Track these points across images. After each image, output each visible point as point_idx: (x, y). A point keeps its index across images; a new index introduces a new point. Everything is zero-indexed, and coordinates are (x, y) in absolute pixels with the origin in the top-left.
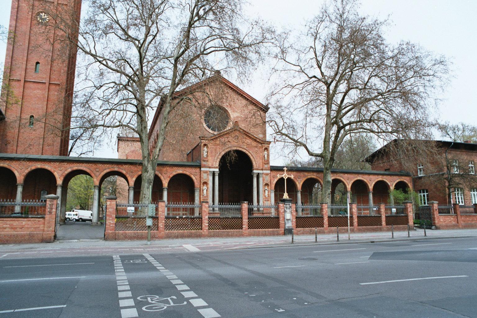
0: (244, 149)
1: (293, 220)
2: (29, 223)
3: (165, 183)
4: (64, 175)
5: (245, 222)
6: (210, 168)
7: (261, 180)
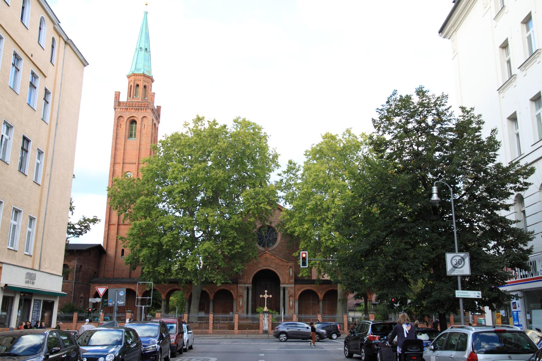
0: (272, 267)
3: (211, 297)
4: (143, 292)
6: (245, 284)
7: (286, 292)
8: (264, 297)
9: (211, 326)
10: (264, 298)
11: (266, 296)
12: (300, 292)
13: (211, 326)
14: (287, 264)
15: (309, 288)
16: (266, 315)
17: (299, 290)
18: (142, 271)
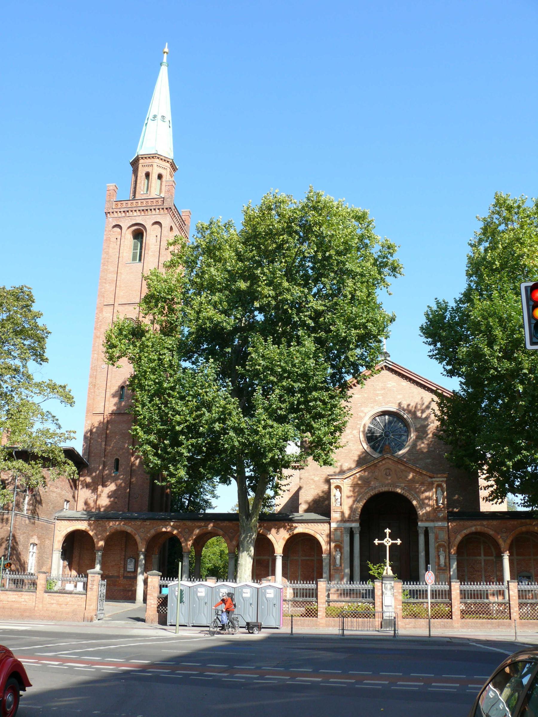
1: (398, 607)
2: (73, 599)
5: (321, 607)
7: (431, 536)
8: (383, 544)
9: (304, 558)
10: (382, 546)
11: (388, 542)
12: (459, 538)
13: (304, 558)
14: (430, 480)
15: (479, 528)
16: (388, 584)
17: (457, 531)
18: (130, 480)
